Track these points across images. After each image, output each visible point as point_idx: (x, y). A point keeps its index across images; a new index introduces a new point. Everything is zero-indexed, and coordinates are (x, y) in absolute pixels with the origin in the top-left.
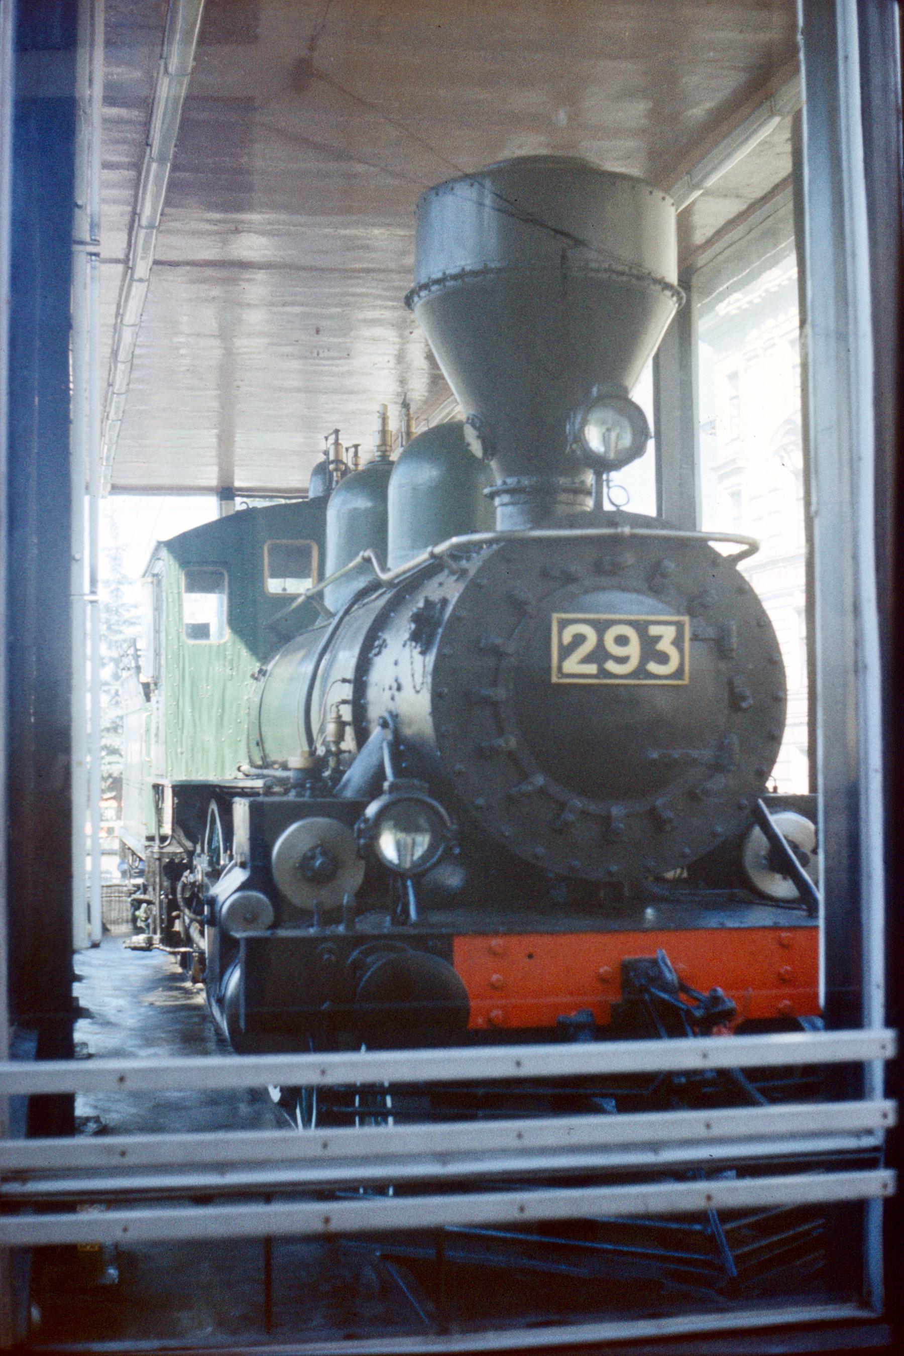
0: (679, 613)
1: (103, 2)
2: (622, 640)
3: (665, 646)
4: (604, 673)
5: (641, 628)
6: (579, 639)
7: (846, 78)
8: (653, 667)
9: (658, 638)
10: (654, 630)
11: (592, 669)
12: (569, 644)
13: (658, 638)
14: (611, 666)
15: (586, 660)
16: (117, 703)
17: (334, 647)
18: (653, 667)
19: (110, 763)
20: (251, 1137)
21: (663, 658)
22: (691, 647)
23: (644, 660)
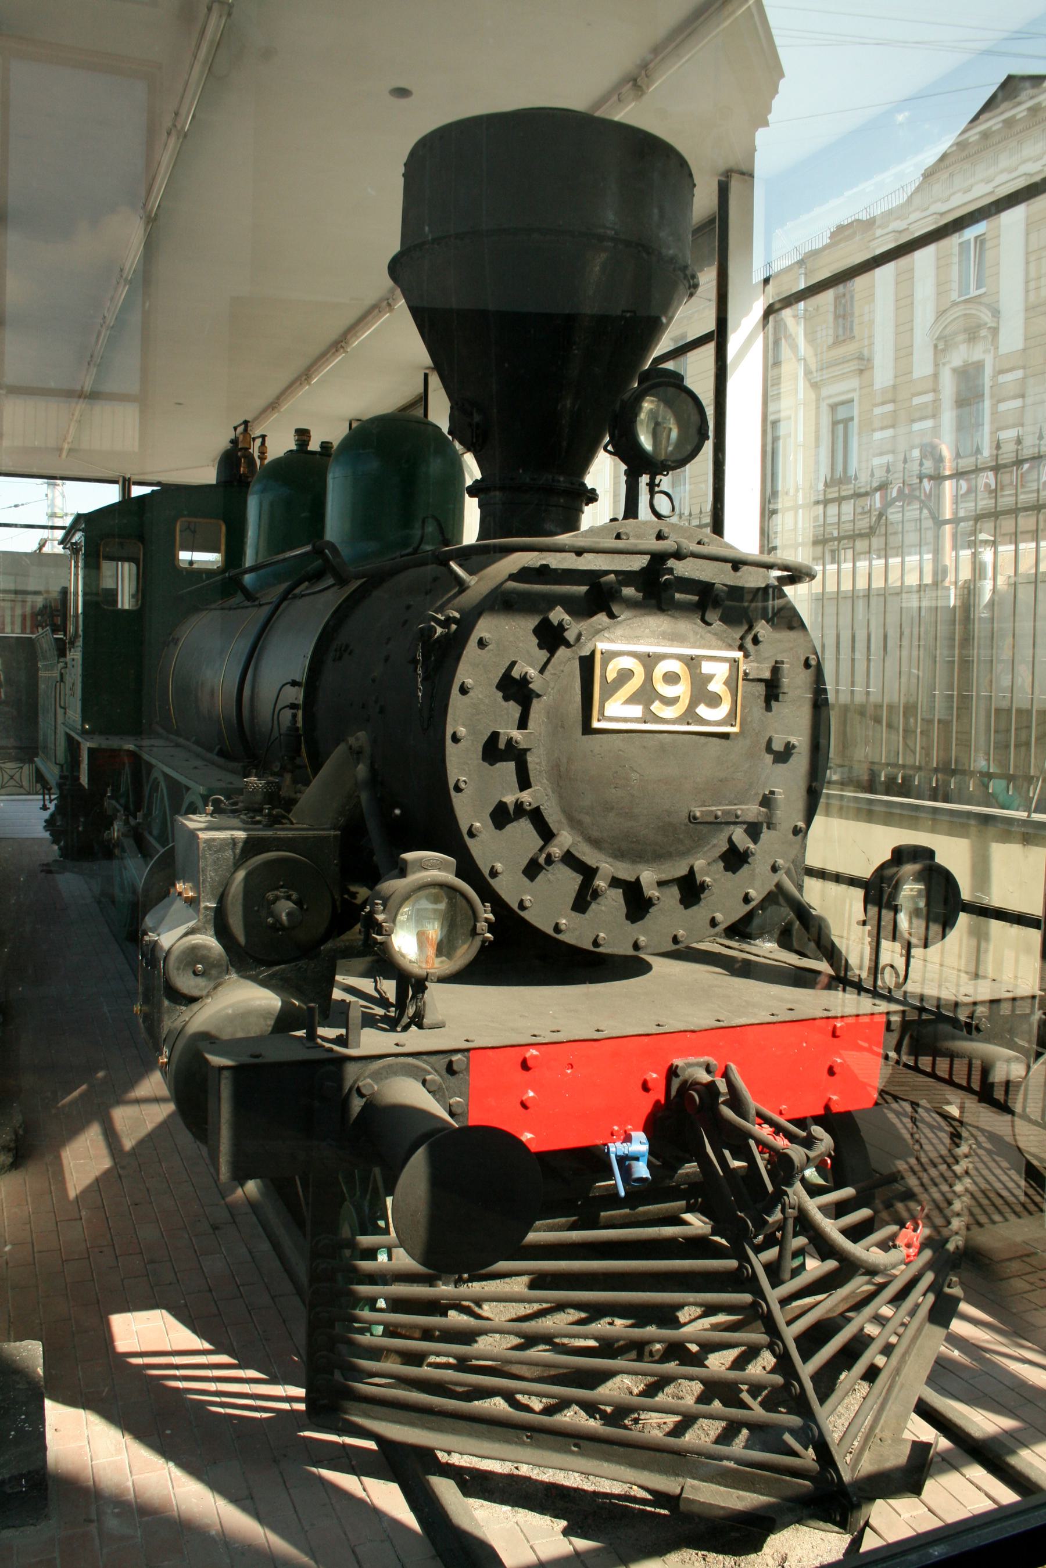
0: (730, 647)
1: (8, 1533)
2: (671, 678)
3: (717, 686)
4: (650, 716)
5: (692, 663)
6: (625, 675)
7: (259, 654)
8: (702, 710)
9: (710, 678)
10: (707, 668)
11: (637, 711)
12: (614, 680)
13: (710, 678)
14: (656, 707)
15: (631, 700)
16: (807, 665)
17: (1029, 515)
18: (702, 710)
19: (99, 334)
20: (222, 1148)
21: (714, 701)
22: (743, 686)
23: (693, 704)
